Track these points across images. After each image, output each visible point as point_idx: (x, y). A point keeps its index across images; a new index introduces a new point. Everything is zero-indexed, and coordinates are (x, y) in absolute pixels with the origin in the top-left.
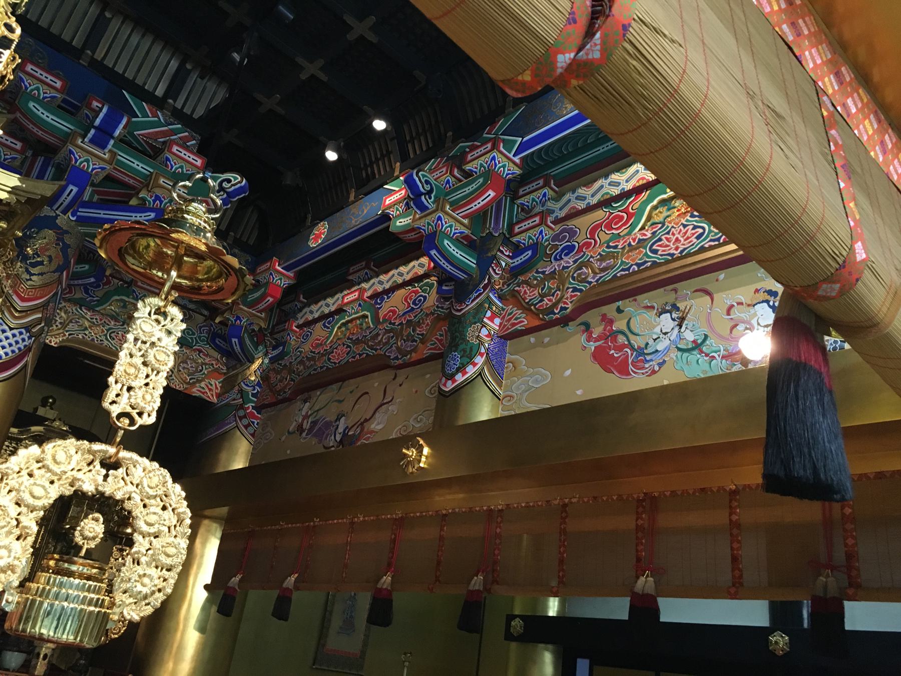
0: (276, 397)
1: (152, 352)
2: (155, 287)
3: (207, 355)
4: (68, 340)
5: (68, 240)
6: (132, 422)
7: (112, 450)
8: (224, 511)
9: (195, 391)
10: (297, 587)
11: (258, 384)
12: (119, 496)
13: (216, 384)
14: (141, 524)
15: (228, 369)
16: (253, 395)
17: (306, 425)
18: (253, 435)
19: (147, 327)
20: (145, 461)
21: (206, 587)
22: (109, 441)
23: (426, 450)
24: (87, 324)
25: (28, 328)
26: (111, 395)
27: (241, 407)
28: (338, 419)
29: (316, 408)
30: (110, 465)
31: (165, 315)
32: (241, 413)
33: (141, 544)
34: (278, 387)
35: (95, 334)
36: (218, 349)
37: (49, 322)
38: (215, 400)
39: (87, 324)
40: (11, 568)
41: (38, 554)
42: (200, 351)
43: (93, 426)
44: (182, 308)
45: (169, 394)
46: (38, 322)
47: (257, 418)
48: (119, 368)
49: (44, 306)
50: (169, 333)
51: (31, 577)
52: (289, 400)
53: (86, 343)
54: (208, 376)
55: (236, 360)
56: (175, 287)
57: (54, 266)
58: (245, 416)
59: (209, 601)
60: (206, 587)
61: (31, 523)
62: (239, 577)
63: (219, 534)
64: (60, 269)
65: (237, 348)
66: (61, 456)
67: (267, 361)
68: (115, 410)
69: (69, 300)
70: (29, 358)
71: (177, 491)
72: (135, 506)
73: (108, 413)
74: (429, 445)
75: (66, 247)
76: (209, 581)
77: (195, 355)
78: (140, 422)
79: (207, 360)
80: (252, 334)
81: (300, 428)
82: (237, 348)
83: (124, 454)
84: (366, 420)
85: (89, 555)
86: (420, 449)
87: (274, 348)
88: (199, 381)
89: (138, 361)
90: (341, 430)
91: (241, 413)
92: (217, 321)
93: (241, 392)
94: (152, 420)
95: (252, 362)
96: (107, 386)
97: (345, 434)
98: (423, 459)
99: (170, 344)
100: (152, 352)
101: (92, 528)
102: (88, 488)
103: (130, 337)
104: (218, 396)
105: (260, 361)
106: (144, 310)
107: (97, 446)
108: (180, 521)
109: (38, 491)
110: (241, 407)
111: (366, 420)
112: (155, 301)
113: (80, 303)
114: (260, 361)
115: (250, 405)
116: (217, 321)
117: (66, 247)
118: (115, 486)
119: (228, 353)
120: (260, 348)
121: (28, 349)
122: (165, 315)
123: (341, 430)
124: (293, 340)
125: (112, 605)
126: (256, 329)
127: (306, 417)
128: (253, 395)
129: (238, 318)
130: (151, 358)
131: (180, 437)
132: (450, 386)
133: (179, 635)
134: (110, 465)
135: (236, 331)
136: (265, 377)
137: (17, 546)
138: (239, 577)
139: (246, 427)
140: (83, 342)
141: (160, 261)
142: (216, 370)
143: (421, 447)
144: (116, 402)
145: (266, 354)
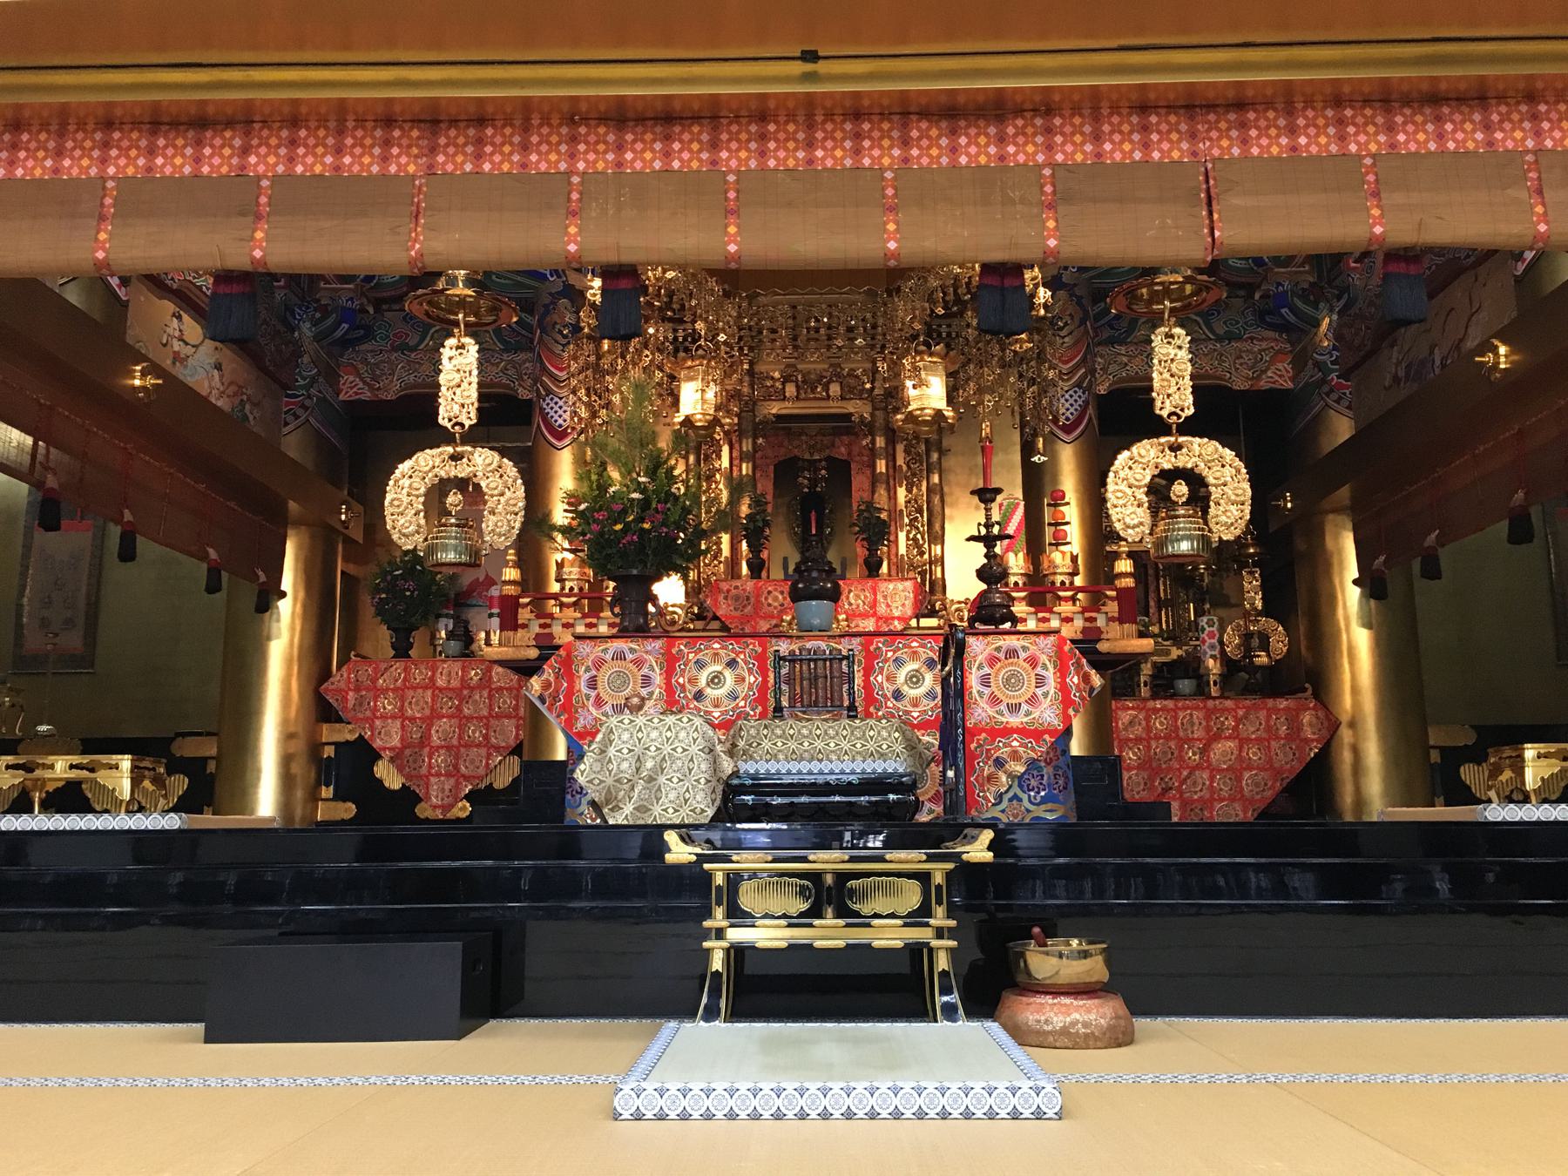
0: (1358, 357)
1: (1173, 366)
2: (1155, 321)
3: (1263, 339)
4: (1114, 383)
5: (1078, 292)
6: (1179, 417)
7: (1172, 439)
8: (1344, 493)
9: (1264, 384)
10: (1441, 541)
11: (1335, 348)
12: (1189, 466)
13: (1285, 366)
14: (1211, 480)
15: (1292, 345)
16: (1333, 363)
17: (1401, 373)
18: (1349, 408)
19: (1164, 351)
20: (1197, 440)
21: (1355, 582)
22: (1170, 434)
23: (1503, 350)
24: (1125, 359)
25: (1079, 385)
26: (1158, 404)
27: (1324, 381)
28: (1432, 352)
29: (1406, 348)
30: (1175, 448)
31: (1172, 336)
32: (1326, 389)
33: (1215, 493)
34: (1357, 342)
35: (1135, 367)
36: (1272, 327)
37: (1092, 372)
38: (1290, 385)
39: (1125, 359)
40: (1141, 524)
41: (1154, 511)
42: (1252, 339)
43: (1156, 427)
44: (1182, 326)
45: (1196, 390)
46: (1084, 377)
47: (1347, 387)
48: (1156, 384)
49: (1084, 360)
50: (1180, 348)
51: (1154, 525)
52: (1373, 353)
53: (1131, 379)
54: (1272, 362)
55: (1298, 332)
56: (1172, 310)
57: (1077, 322)
58: (1332, 391)
59: (1363, 595)
60: (1355, 582)
61: (1141, 495)
62: (1382, 558)
63: (1350, 525)
64: (1083, 322)
65: (1292, 318)
66: (1143, 452)
67: (1335, 317)
68: (1165, 413)
69: (1099, 344)
70: (1090, 411)
71: (1229, 454)
72: (1202, 468)
73: (1160, 417)
74: (1504, 343)
75: (1079, 298)
76: (1356, 575)
77: (1246, 346)
78: (1184, 415)
79: (1264, 345)
80: (1304, 295)
81: (1396, 379)
82: (1292, 318)
83: (1181, 439)
84: (1461, 340)
85: (1184, 504)
86: (1495, 350)
87: (1339, 298)
88: (1265, 372)
89: (1166, 375)
90: (1438, 363)
91: (1326, 389)
92: (1257, 296)
93: (1317, 364)
94: (1192, 410)
95: (1318, 325)
96: (1153, 400)
97: (1443, 366)
98: (1502, 359)
99: (1184, 355)
100: (1173, 366)
101: (1180, 489)
102: (1167, 466)
103: (1155, 361)
104: (1292, 379)
105: (1327, 320)
106: (1157, 339)
107: (1163, 440)
108: (1238, 471)
109: (1139, 477)
110: (1324, 381)
111: (1461, 340)
112: (1163, 329)
113: (1111, 342)
114: (1327, 320)
115: (1334, 375)
116: (1257, 296)
117: (1079, 303)
118: (1184, 461)
119: (1284, 327)
120: (1322, 305)
121: (1086, 403)
122: (1172, 336)
123: (1438, 363)
124: (1356, 279)
125: (1210, 531)
126: (1306, 286)
127: (1399, 363)
128: (1333, 363)
129: (1279, 284)
130: (1174, 370)
131: (1215, 413)
132: (1521, 267)
133: (1344, 637)
134: (1175, 448)
135: (1282, 300)
136: (1338, 334)
137: (1139, 510)
138: (1382, 558)
139: (1337, 401)
140: (1130, 379)
141: (1156, 297)
142: (1279, 352)
143: (1497, 347)
144: (1163, 407)
145: (1331, 310)
